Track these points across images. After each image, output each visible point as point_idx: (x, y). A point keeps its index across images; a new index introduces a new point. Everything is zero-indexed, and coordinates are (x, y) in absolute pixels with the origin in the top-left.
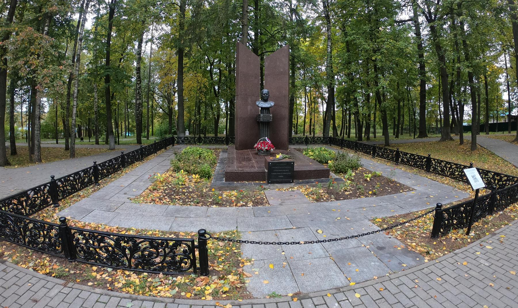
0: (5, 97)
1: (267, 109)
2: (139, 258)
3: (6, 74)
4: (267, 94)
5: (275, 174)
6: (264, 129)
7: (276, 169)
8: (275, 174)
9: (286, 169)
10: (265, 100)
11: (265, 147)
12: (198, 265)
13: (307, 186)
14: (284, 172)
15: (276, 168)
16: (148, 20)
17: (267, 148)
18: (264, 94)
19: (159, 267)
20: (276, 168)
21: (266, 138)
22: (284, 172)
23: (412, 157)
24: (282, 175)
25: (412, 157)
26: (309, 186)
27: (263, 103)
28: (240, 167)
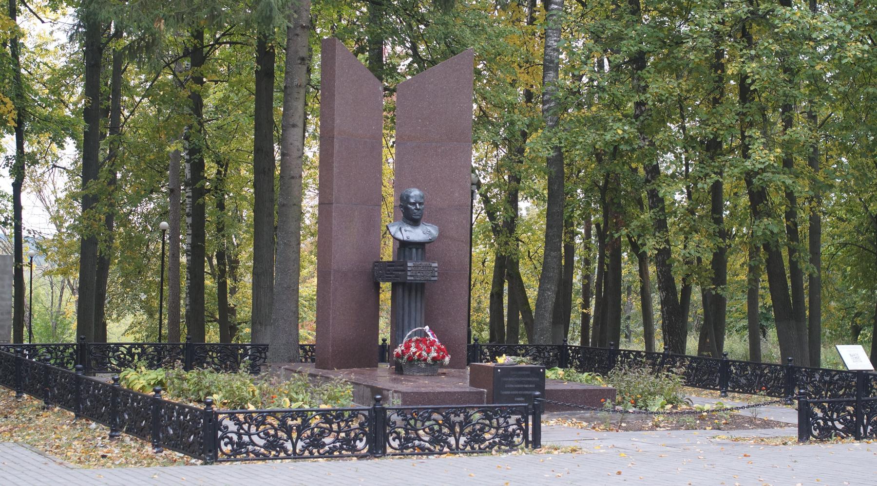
0: (565, 252)
1: (420, 246)
2: (470, 433)
3: (768, 267)
4: (420, 204)
5: (508, 393)
6: (413, 305)
7: (511, 383)
8: (508, 393)
9: (529, 383)
10: (413, 221)
11: (429, 352)
12: (530, 439)
13: (574, 420)
14: (526, 389)
15: (510, 379)
16: (520, 194)
17: (435, 354)
18: (414, 204)
19: (490, 443)
20: (510, 379)
21: (427, 328)
22: (526, 389)
23: (827, 378)
24: (523, 396)
25: (827, 378)
26: (577, 418)
27: (409, 228)
28: (416, 387)
